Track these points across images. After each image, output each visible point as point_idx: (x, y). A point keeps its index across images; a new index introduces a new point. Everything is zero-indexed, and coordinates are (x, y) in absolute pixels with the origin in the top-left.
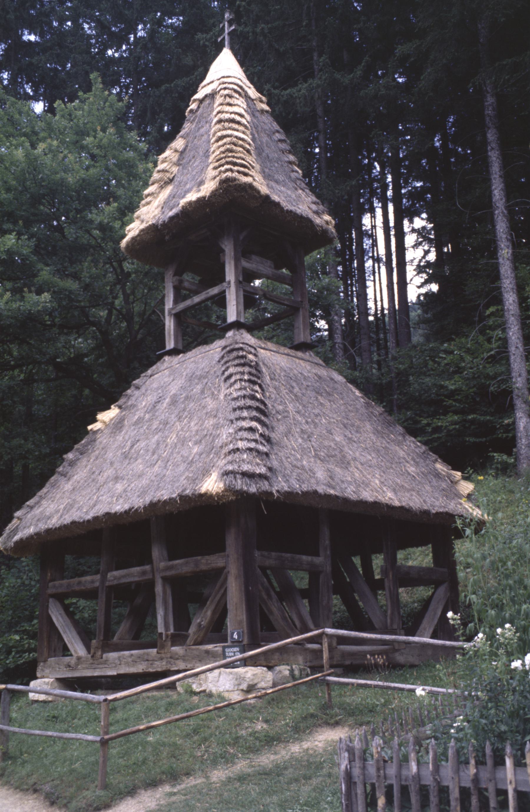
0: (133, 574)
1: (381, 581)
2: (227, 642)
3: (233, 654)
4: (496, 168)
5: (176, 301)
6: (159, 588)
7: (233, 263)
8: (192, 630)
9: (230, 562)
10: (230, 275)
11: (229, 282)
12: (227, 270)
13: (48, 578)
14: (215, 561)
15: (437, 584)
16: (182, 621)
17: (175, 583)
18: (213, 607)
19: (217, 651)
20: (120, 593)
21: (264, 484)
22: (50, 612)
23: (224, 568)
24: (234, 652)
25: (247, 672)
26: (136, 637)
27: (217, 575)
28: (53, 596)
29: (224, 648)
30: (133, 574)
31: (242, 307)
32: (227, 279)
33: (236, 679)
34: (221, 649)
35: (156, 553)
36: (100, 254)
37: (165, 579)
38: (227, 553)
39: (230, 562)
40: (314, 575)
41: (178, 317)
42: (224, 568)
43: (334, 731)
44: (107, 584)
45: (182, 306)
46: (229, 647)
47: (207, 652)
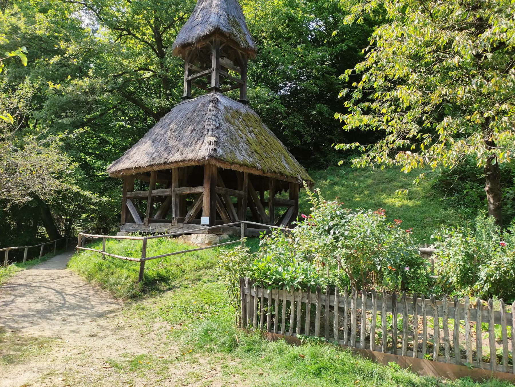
1: (268, 203)
4: (174, 209)
8: (187, 217)
10: (214, 65)
12: (213, 61)
14: (199, 190)
15: (290, 206)
16: (183, 212)
18: (194, 210)
20: (160, 199)
21: (424, 323)
26: (164, 218)
27: (198, 196)
30: (166, 192)
31: (218, 81)
32: (213, 67)
39: (204, 191)
40: (240, 199)
41: (189, 82)
47: (193, 227)
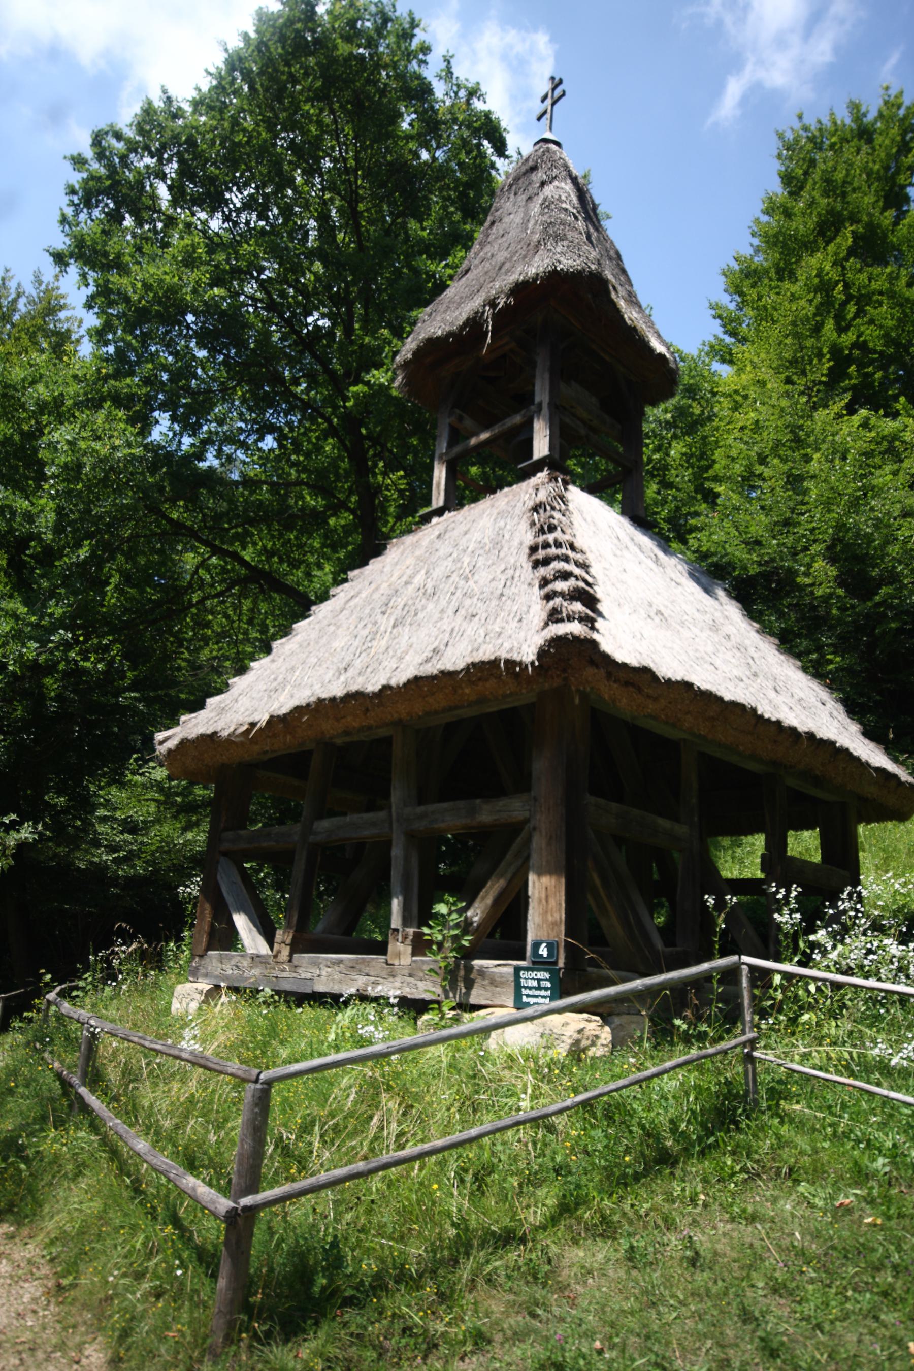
0: (358, 825)
2: (523, 959)
3: (535, 984)
5: (450, 446)
6: (397, 852)
7: (547, 376)
9: (537, 811)
11: (540, 404)
13: (222, 825)
14: (514, 808)
17: (427, 846)
19: (501, 975)
22: (219, 878)
23: (527, 821)
24: (539, 980)
25: (565, 1024)
26: (348, 932)
28: (225, 854)
29: (517, 970)
30: (358, 825)
32: (537, 399)
33: (542, 1036)
34: (511, 970)
35: (396, 796)
36: (159, 305)
37: (411, 837)
38: (533, 793)
42: (527, 821)
43: (782, 657)
44: (311, 839)
45: (457, 449)
46: (527, 969)
